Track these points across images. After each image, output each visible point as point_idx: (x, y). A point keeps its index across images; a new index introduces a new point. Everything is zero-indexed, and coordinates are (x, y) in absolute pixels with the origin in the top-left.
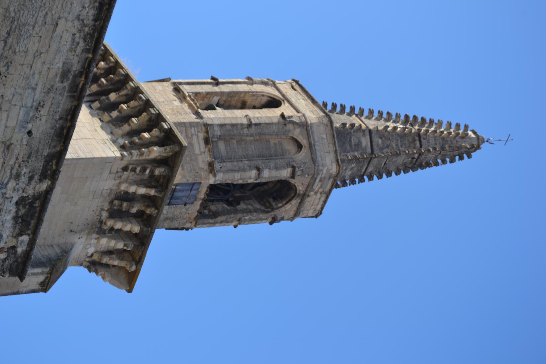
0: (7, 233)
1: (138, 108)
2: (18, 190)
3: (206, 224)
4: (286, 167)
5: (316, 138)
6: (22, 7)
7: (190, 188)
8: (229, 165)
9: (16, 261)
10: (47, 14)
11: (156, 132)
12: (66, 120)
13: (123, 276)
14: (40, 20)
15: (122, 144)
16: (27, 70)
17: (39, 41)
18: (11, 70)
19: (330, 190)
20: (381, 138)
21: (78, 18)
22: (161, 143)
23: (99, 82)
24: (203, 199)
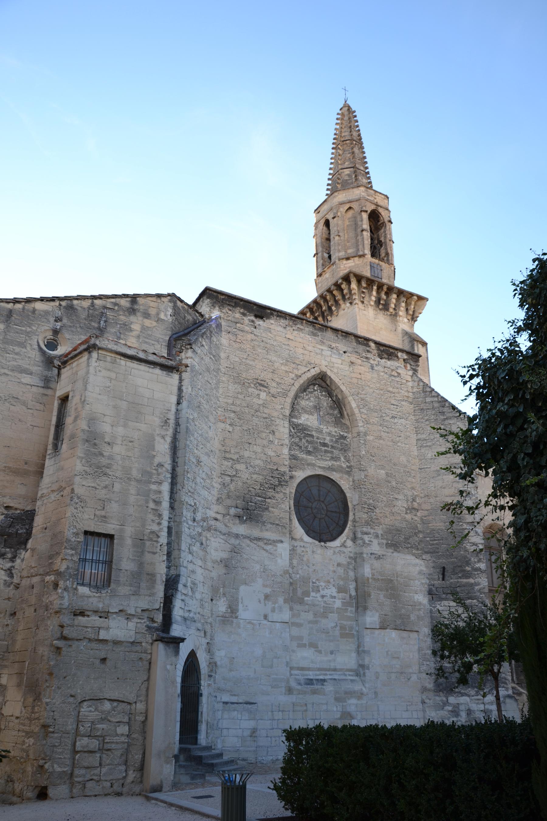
5: (346, 199)
8: (361, 247)
11: (344, 286)
12: (338, 333)
13: (420, 303)
14: (287, 347)
16: (312, 354)
18: (313, 362)
21: (285, 328)
22: (349, 282)
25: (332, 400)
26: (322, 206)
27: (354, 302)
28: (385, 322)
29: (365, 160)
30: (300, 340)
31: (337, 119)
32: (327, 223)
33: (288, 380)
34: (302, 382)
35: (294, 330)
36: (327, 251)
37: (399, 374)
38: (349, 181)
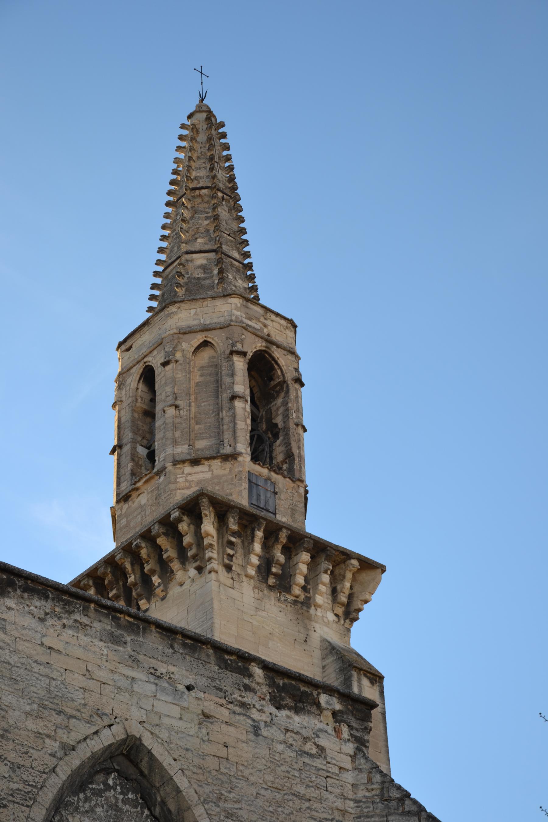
0: (317, 722)
2: (262, 706)
3: (301, 467)
4: (231, 363)
5: (195, 322)
6: (25, 693)
7: (255, 486)
8: (227, 436)
10: (36, 662)
11: (183, 527)
12: (174, 639)
13: (365, 576)
14: (44, 670)
15: (196, 572)
16: (108, 689)
18: (108, 711)
20: (196, 239)
21: (42, 620)
22: (197, 519)
24: (270, 470)
25: (152, 814)
26: (137, 336)
27: (209, 567)
28: (282, 618)
29: (244, 237)
30: (79, 652)
31: (181, 138)
32: (148, 376)
33: (42, 758)
34: (77, 763)
35: (64, 626)
36: (145, 442)
37: (322, 749)
38: (203, 282)
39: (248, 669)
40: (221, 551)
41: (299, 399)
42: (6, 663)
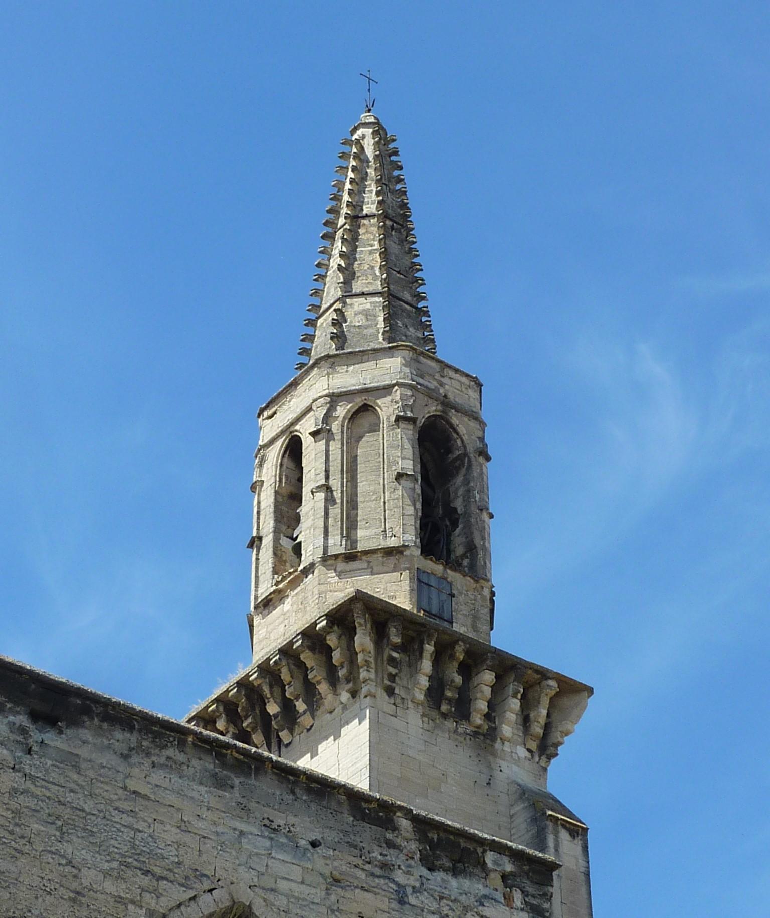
0: (481, 887)
1: (292, 667)
2: (409, 866)
3: (485, 563)
9: (527, 874)
10: (116, 809)
11: (332, 640)
12: (295, 783)
13: (566, 701)
14: (127, 819)
16: (209, 844)
17: (162, 823)
19: (438, 361)
21: (125, 757)
22: (349, 631)
23: (248, 730)
30: (172, 798)
39: (392, 820)
40: (380, 671)
41: (485, 477)
42: (79, 810)
